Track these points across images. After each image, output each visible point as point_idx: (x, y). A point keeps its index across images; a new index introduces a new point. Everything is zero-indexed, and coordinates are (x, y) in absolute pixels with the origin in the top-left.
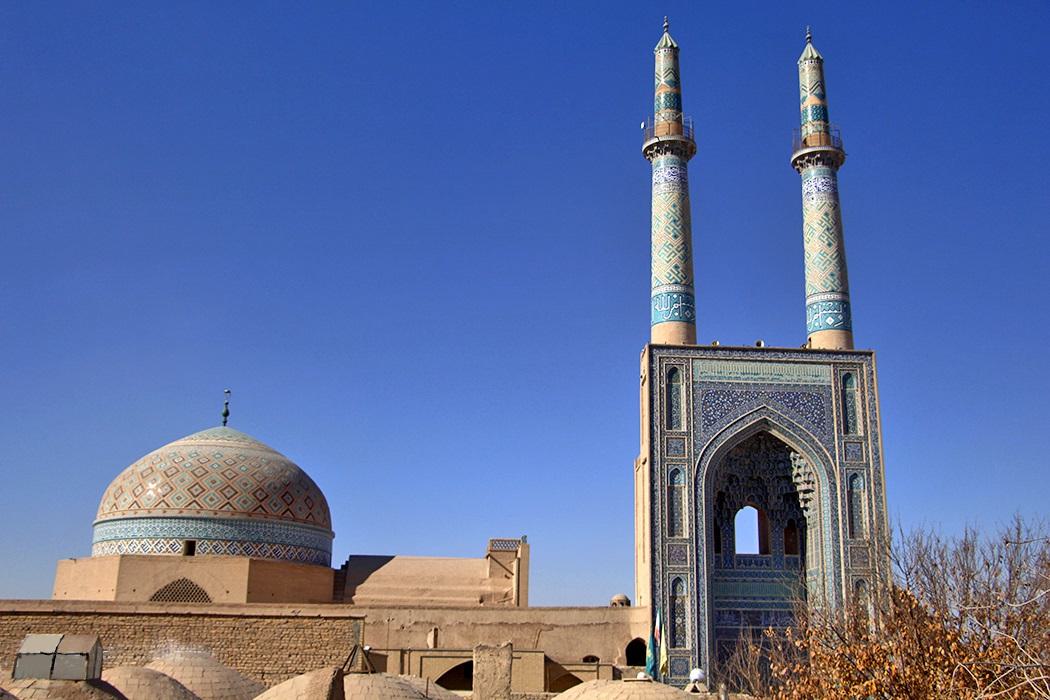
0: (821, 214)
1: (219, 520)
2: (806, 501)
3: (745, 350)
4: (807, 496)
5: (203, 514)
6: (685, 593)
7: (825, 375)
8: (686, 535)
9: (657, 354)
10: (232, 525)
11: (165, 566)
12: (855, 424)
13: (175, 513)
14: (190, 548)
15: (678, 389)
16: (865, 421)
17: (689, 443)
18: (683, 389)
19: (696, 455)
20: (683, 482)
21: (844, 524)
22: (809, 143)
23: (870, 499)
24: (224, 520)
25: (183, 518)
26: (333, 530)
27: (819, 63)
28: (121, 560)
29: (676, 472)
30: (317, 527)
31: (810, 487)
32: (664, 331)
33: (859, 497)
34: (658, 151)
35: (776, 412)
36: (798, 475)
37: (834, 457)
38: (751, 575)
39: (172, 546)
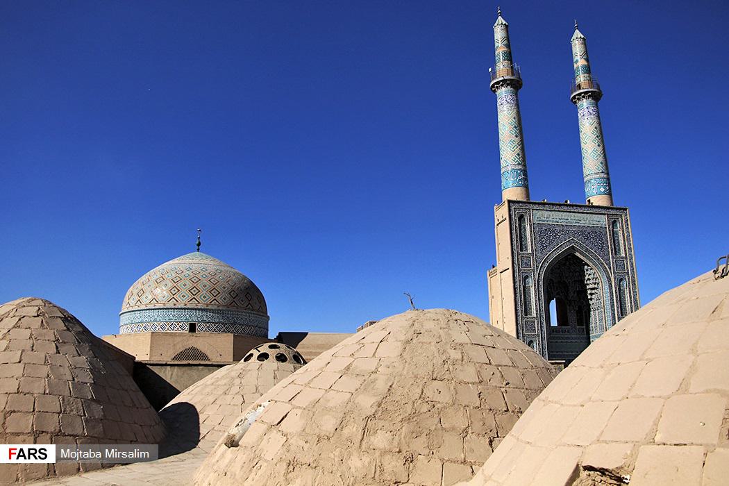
0: (593, 127)
1: (210, 310)
2: (591, 294)
3: (560, 205)
4: (593, 292)
5: (200, 306)
7: (603, 221)
8: (534, 315)
11: (178, 339)
12: (619, 250)
13: (182, 306)
14: (192, 328)
16: (625, 248)
17: (533, 260)
18: (528, 227)
19: (537, 267)
20: (531, 283)
21: (618, 308)
22: (582, 87)
23: (630, 293)
25: (188, 309)
26: (268, 314)
27: (585, 42)
28: (152, 336)
29: (527, 277)
30: (259, 313)
31: (596, 286)
32: (512, 191)
33: (624, 291)
34: (584, 97)
35: (578, 242)
36: (589, 279)
37: (610, 268)
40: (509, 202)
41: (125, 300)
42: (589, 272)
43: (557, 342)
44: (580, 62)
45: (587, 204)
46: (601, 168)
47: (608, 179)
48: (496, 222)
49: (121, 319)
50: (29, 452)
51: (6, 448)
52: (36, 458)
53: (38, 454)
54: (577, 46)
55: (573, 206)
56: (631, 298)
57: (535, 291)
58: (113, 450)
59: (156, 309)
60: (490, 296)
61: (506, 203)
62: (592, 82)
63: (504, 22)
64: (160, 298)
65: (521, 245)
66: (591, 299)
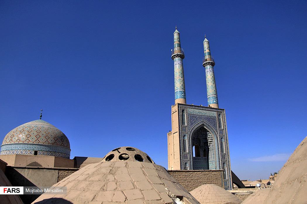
2: (210, 144)
3: (199, 107)
4: (211, 143)
5: (40, 143)
6: (188, 166)
7: (215, 114)
9: (180, 106)
10: (48, 147)
12: (221, 126)
14: (36, 153)
15: (184, 115)
18: (186, 115)
20: (186, 138)
22: (207, 60)
23: (225, 144)
24: (46, 145)
25: (34, 144)
27: (209, 43)
28: (16, 156)
29: (185, 136)
32: (179, 100)
34: (208, 64)
35: (206, 122)
36: (209, 138)
37: (218, 133)
38: (196, 162)
39: (30, 152)
40: (178, 104)
41: (4, 139)
42: (209, 135)
43: (195, 163)
44: (207, 51)
45: (208, 107)
46: (214, 93)
47: (217, 97)
48: (172, 113)
49: (2, 148)
50: (12, 190)
51: (2, 188)
52: (15, 192)
53: (16, 191)
54: (206, 45)
55: (203, 107)
56: (225, 146)
57: (188, 142)
58: (47, 189)
59: (19, 144)
60: (168, 144)
61: (177, 104)
62: (211, 59)
63: (178, 32)
64: (21, 139)
65: (183, 122)
66: (210, 146)
